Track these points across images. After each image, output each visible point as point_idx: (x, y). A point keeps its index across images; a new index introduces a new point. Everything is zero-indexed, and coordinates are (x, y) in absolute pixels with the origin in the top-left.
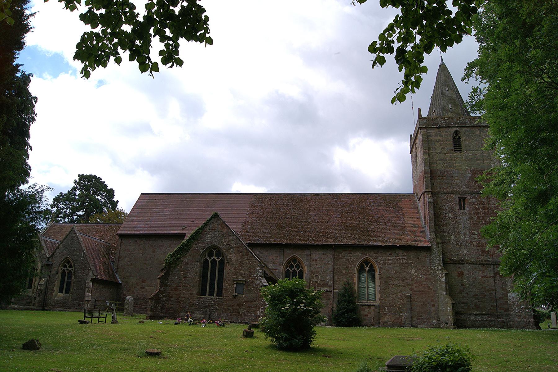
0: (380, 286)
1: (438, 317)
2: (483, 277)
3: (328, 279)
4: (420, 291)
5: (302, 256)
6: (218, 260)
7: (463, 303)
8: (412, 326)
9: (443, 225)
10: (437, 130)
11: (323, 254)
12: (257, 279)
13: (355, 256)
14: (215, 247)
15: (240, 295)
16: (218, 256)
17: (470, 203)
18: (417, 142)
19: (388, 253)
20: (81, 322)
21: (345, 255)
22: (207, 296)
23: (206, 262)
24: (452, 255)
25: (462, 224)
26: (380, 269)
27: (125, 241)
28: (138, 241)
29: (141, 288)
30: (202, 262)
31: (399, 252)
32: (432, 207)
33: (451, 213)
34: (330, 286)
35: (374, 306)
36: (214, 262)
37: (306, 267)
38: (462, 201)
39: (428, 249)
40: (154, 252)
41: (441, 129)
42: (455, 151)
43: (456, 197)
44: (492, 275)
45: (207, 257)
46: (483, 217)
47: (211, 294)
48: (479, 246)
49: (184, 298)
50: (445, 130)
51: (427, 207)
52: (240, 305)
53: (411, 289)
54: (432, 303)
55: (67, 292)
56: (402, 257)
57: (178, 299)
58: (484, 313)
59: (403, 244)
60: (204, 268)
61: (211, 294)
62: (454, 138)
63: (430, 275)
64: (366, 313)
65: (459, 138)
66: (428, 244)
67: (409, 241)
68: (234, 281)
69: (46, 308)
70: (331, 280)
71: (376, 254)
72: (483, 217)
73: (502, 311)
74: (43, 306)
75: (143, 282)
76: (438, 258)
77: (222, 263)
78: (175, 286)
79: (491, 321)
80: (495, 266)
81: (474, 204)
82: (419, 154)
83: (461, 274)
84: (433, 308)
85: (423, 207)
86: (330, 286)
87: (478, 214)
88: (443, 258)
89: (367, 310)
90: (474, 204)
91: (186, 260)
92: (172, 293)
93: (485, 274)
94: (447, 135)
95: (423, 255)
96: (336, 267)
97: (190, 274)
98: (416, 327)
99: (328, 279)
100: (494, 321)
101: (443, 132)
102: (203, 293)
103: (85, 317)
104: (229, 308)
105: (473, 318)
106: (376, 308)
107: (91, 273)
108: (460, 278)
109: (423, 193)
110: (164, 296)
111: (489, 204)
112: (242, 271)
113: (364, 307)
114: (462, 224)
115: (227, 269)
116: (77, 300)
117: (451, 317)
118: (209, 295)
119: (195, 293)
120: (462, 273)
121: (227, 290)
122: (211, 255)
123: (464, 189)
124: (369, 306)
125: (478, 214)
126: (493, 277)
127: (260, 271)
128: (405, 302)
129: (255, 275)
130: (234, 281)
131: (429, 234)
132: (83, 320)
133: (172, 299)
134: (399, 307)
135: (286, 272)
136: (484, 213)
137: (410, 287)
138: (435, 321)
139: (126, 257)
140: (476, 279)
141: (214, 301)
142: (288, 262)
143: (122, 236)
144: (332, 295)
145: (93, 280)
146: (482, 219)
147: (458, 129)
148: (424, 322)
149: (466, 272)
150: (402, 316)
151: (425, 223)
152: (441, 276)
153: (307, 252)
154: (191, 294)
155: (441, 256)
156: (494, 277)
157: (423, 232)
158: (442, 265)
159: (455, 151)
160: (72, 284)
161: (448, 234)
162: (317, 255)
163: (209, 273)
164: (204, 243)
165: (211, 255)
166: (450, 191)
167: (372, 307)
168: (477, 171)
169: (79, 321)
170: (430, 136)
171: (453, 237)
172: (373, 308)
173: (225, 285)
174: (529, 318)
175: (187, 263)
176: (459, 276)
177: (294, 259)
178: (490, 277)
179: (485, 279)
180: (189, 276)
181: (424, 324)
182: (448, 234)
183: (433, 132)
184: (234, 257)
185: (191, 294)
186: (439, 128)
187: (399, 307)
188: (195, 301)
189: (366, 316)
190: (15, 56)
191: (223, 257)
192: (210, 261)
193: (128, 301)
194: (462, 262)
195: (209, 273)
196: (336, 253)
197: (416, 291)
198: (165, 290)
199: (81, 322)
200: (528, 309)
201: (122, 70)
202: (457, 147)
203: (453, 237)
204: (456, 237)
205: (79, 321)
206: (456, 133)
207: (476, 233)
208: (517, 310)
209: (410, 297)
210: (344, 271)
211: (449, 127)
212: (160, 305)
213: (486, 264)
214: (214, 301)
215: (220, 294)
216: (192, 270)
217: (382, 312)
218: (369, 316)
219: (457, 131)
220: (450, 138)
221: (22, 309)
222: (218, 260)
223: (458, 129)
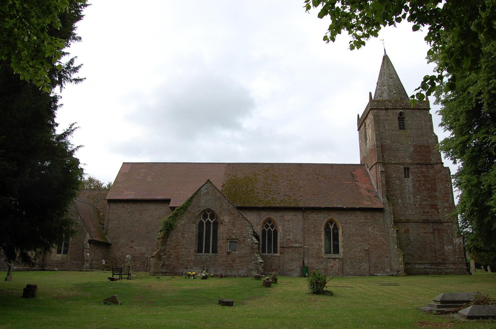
0: (343, 242)
1: (391, 266)
2: (425, 233)
3: (299, 237)
4: (376, 245)
5: (275, 216)
6: (212, 222)
7: (410, 255)
8: (371, 275)
9: (392, 191)
10: (384, 111)
11: (294, 215)
12: (248, 238)
13: (321, 217)
14: (209, 210)
15: (234, 252)
16: (212, 218)
17: (413, 172)
18: (368, 121)
19: (349, 214)
20: (112, 279)
21: (313, 216)
22: (203, 254)
23: (201, 224)
24: (400, 215)
25: (407, 190)
26: (343, 227)
27: (113, 206)
28: (126, 205)
29: (130, 248)
30: (198, 223)
31: (358, 213)
32: (384, 175)
33: (398, 180)
34: (301, 243)
35: (339, 258)
36: (208, 223)
37: (280, 227)
38: (407, 170)
39: (381, 210)
40: (141, 215)
41: (389, 111)
42: (400, 129)
43: (402, 167)
44: (432, 231)
45: (202, 219)
46: (424, 184)
47: (207, 251)
48: (421, 208)
49: (183, 255)
50: (392, 111)
51: (379, 176)
52: (233, 260)
53: (369, 244)
54: (386, 255)
55: (65, 252)
56: (361, 217)
57: (177, 257)
58: (426, 262)
59: (361, 206)
60: (199, 229)
61: (207, 251)
62: (399, 118)
63: (383, 232)
64: (332, 265)
65: (403, 118)
66: (381, 206)
67: (367, 204)
68: (228, 239)
69: (45, 268)
70: (301, 238)
71: (339, 215)
72: (424, 184)
73: (440, 260)
74: (43, 267)
75: (132, 242)
76: (389, 219)
77: (216, 224)
78: (174, 245)
79: (432, 268)
80: (434, 224)
81: (417, 173)
82: (370, 132)
83: (407, 231)
84: (387, 259)
85: (374, 176)
86: (301, 243)
87: (419, 181)
88: (394, 217)
89: (332, 262)
90: (417, 173)
91: (183, 222)
92: (172, 251)
93: (426, 231)
94: (393, 116)
95: (378, 215)
96: (306, 226)
97: (187, 234)
98: (373, 275)
99: (299, 237)
100: (435, 268)
101: (390, 113)
102: (199, 250)
103: (113, 274)
104: (225, 263)
105: (417, 266)
106: (340, 261)
107: (88, 235)
108: (407, 234)
109: (376, 164)
110: (165, 254)
111: (428, 173)
112: (234, 231)
113: (330, 259)
114: (407, 190)
115: (221, 229)
116: (75, 260)
117: (402, 266)
118: (205, 252)
119: (192, 251)
120: (408, 230)
121: (221, 247)
122: (205, 217)
123: (408, 161)
124: (335, 259)
125: (419, 181)
126: (432, 233)
127: (251, 230)
128: (364, 255)
129: (246, 234)
130: (228, 239)
131: (381, 199)
132: (111, 277)
133: (172, 256)
134: (359, 259)
135: (262, 231)
136: (425, 181)
137: (368, 242)
138: (388, 270)
139: (114, 220)
140: (419, 234)
141: (210, 257)
142: (265, 223)
143: (110, 201)
144: (303, 250)
145: (90, 242)
146: (422, 186)
147: (402, 111)
148: (380, 271)
149: (411, 229)
150: (362, 266)
151: (377, 188)
152: (392, 231)
153: (280, 214)
154: (189, 252)
155: (392, 216)
156: (433, 233)
157: (376, 196)
158: (393, 223)
159: (400, 129)
160: (70, 246)
161: (396, 197)
162: (289, 216)
163: (204, 233)
164: (199, 207)
165: (205, 217)
166: (397, 162)
167: (336, 260)
168: (418, 146)
169: (109, 278)
170: (380, 116)
171: (400, 201)
172: (337, 260)
173: (220, 243)
174: (462, 265)
175: (185, 224)
176: (405, 233)
177: (269, 220)
178: (430, 233)
179: (426, 234)
180: (187, 236)
181: (380, 273)
182: (396, 197)
183: (383, 113)
184: (226, 219)
185: (189, 252)
186: (387, 109)
187: (359, 259)
188: (193, 258)
189: (332, 267)
190: (82, 18)
191: (217, 219)
192: (204, 222)
193: (128, 259)
194: (408, 221)
195: (204, 233)
196: (306, 214)
197: (373, 245)
198: (165, 249)
199: (112, 279)
200: (462, 258)
201: (72, 58)
202: (402, 126)
203: (400, 201)
204: (402, 200)
205: (109, 278)
206: (401, 114)
207: (418, 197)
208: (452, 259)
209: (368, 250)
210: (312, 230)
211: (395, 109)
212: (162, 262)
213: (427, 223)
214: (210, 257)
215: (215, 251)
216: (187, 230)
217: (346, 263)
218: (335, 267)
219: (401, 113)
220: (396, 118)
221: (20, 270)
222: (212, 222)
223: (402, 111)
